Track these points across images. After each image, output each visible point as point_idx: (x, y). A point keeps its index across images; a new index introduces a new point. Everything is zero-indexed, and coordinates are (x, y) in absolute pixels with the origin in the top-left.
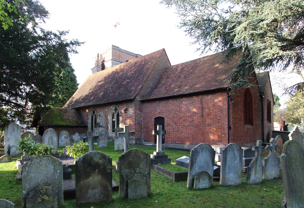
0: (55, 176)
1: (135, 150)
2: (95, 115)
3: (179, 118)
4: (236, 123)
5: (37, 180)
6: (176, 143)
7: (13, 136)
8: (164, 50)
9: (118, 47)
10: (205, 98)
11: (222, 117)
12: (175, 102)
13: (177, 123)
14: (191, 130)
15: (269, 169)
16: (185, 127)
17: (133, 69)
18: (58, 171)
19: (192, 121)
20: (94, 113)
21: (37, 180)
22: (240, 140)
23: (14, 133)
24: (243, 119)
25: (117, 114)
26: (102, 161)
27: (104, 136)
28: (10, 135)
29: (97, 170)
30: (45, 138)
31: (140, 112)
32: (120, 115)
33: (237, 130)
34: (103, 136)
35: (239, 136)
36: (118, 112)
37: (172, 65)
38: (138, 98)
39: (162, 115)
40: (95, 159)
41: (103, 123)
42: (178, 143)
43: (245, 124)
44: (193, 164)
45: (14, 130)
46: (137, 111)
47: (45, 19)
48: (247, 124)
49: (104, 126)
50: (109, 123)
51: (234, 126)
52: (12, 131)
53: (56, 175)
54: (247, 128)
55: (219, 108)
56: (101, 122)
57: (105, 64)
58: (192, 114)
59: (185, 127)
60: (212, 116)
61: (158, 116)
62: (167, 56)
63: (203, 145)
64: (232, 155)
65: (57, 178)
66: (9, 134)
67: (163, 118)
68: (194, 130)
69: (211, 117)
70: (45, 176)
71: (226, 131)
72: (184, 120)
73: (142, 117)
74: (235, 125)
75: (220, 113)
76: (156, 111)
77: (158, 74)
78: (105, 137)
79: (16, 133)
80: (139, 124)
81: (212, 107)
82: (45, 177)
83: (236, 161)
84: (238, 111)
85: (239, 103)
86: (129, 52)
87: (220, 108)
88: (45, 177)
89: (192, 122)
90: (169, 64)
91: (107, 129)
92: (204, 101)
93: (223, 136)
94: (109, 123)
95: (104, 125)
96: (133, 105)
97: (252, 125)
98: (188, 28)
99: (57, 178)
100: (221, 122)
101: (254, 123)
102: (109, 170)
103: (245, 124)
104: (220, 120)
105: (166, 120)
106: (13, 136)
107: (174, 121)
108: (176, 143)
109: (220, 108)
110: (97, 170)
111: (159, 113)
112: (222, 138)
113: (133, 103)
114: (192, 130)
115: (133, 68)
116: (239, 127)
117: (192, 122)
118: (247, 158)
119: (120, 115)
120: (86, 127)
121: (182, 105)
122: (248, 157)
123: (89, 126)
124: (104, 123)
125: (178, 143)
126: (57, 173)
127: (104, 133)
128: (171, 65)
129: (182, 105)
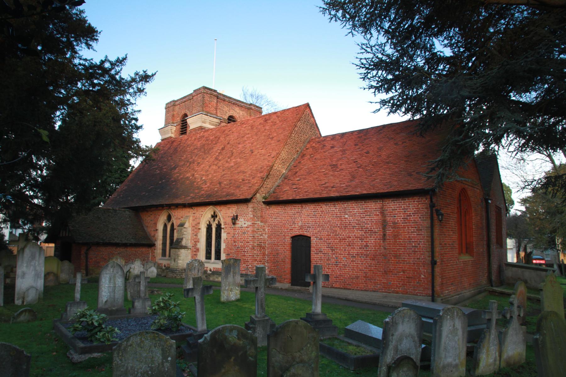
0: (163, 366)
1: (294, 321)
2: (170, 223)
3: (340, 239)
4: (446, 254)
5: (136, 373)
6: (334, 288)
7: (32, 268)
8: (308, 105)
9: (215, 91)
10: (389, 205)
11: (421, 242)
12: (333, 208)
13: (336, 248)
14: (362, 264)
15: (509, 348)
16: (352, 257)
17: (247, 138)
18: (169, 359)
19: (365, 246)
20: (169, 218)
21: (136, 373)
22: (452, 284)
23: (33, 263)
24: (456, 245)
25: (217, 225)
26: (241, 342)
27: (196, 271)
28: (27, 266)
29: (233, 358)
30: (103, 280)
31: (262, 224)
32: (222, 226)
33: (447, 266)
34: (194, 270)
35: (450, 277)
36: (219, 222)
37: (323, 135)
38: (259, 197)
39: (306, 232)
40: (230, 339)
41: (187, 240)
42: (336, 288)
43: (461, 252)
44: (389, 345)
45: (33, 257)
46: (257, 222)
47: (93, 44)
48: (462, 253)
49: (190, 248)
50: (199, 242)
51: (442, 259)
52: (30, 259)
53: (165, 364)
54: (463, 262)
55: (415, 225)
56: (184, 240)
57: (187, 120)
58: (365, 233)
59: (352, 257)
60: (402, 239)
61: (297, 233)
62: (313, 117)
63: (404, 312)
64: (450, 328)
65: (166, 370)
66: (25, 265)
67: (308, 238)
68: (368, 264)
69: (399, 242)
70: (149, 367)
71: (417, 256)
72: (349, 244)
73: (266, 234)
74: (444, 256)
75: (417, 235)
76: (294, 223)
77: (298, 151)
78: (198, 272)
79: (37, 263)
80: (261, 246)
81: (402, 223)
82: (148, 369)
83: (456, 338)
84: (449, 230)
85: (449, 217)
86: (235, 100)
87: (417, 225)
88: (148, 369)
89: (364, 248)
90: (318, 133)
91: (194, 253)
92: (387, 210)
93: (423, 278)
94: (199, 242)
95: (190, 245)
96: (250, 209)
97: (471, 256)
98: (373, 90)
99: (166, 370)
100: (420, 251)
101: (475, 250)
102: (252, 357)
103: (461, 252)
104: (417, 247)
105: (314, 241)
106: (32, 268)
107: (330, 243)
108: (334, 288)
109: (417, 225)
110: (233, 358)
111: (301, 228)
112: (421, 281)
113: (250, 205)
114: (365, 264)
115: (247, 136)
116: (451, 261)
117: (364, 248)
118: (472, 328)
119: (223, 228)
120: (152, 245)
121: (346, 216)
122: (473, 325)
123: (159, 244)
124: (190, 241)
125: (336, 288)
126: (167, 361)
127: (197, 264)
128: (320, 135)
129: (346, 216)
